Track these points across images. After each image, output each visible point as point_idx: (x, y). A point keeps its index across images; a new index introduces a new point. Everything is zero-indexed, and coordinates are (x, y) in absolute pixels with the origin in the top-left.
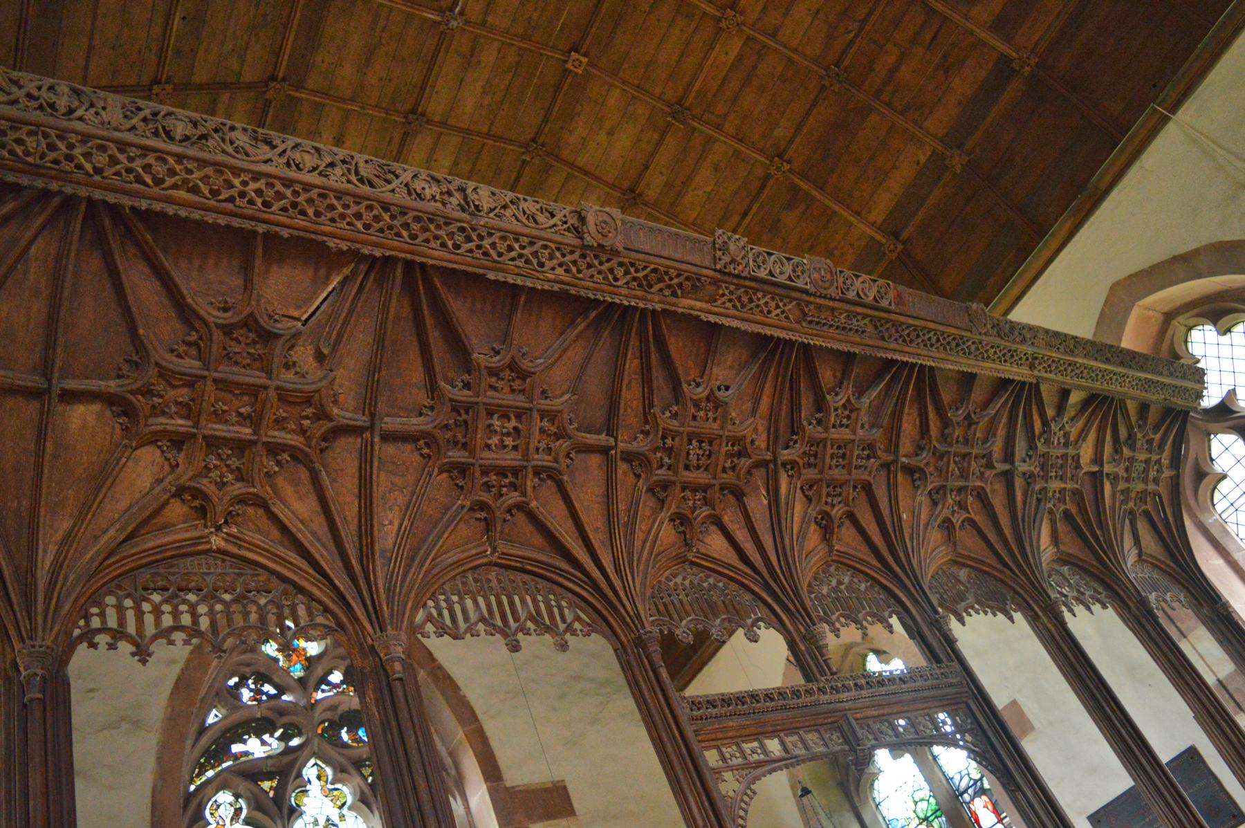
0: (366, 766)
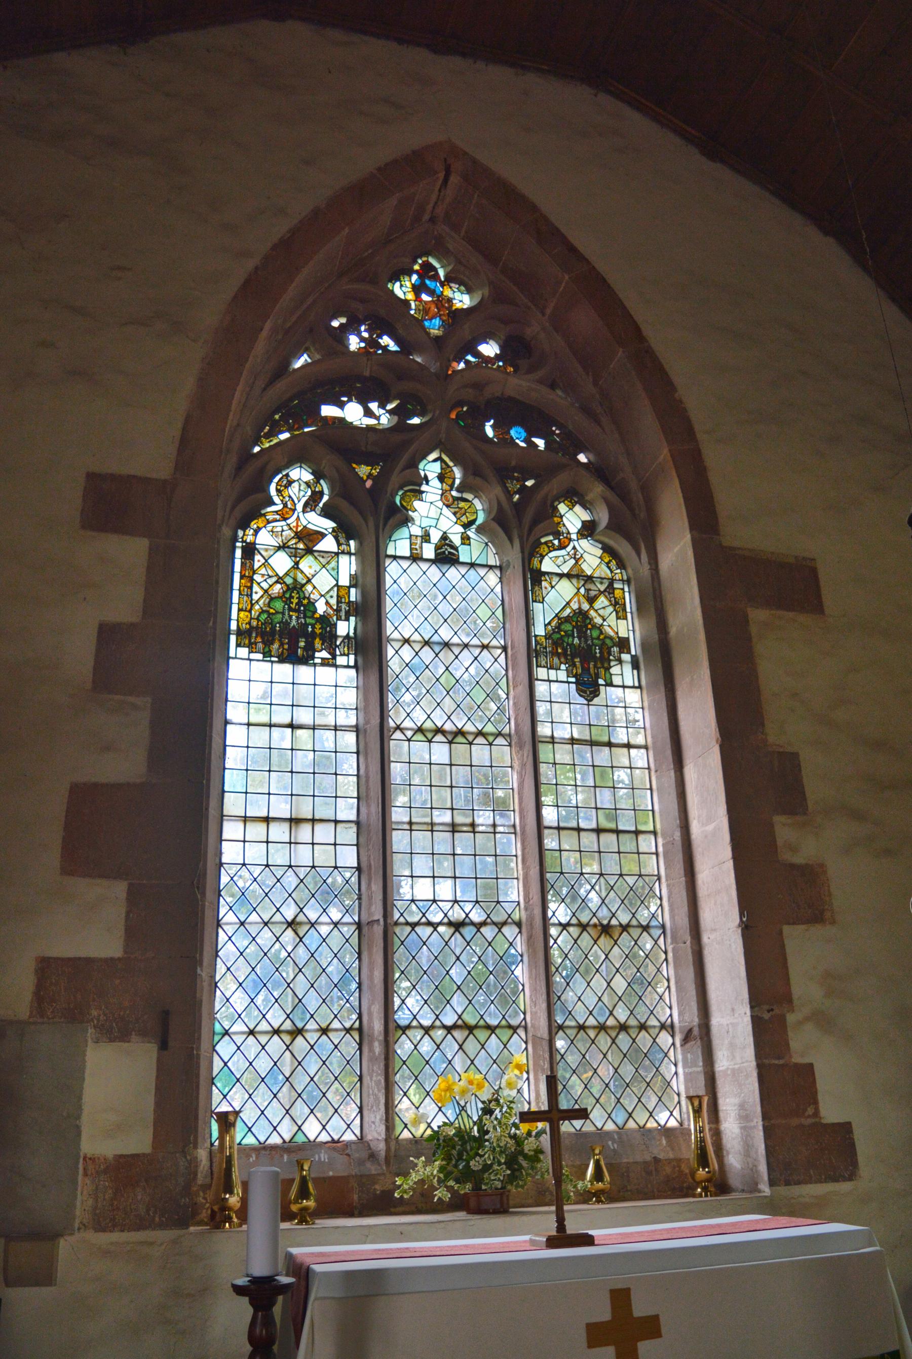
0: (513, 478)
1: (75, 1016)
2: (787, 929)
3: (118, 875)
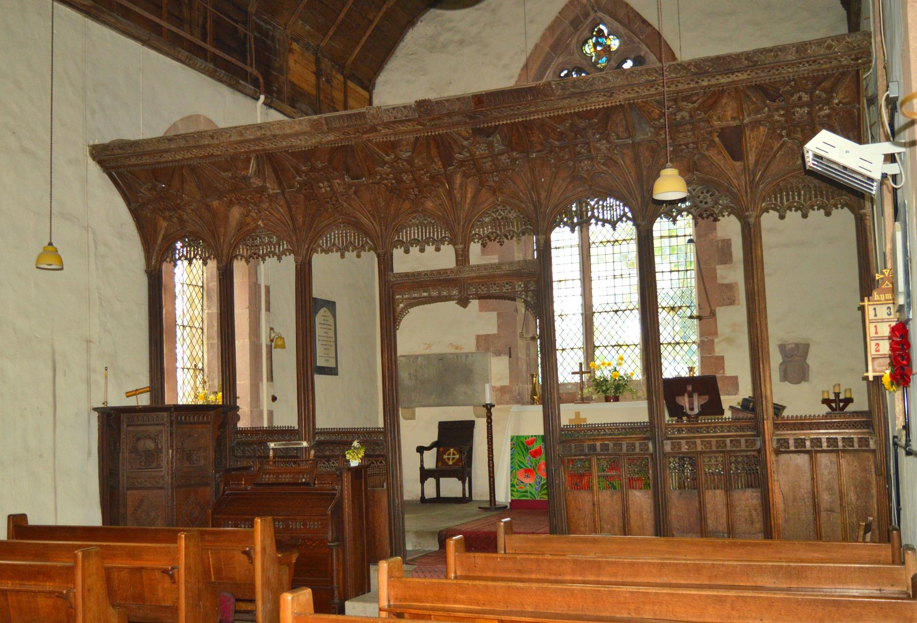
1: (487, 349)
3: (494, 310)
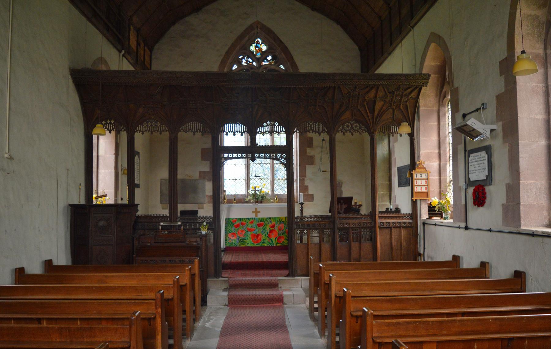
1: (204, 178)
2: (307, 166)
